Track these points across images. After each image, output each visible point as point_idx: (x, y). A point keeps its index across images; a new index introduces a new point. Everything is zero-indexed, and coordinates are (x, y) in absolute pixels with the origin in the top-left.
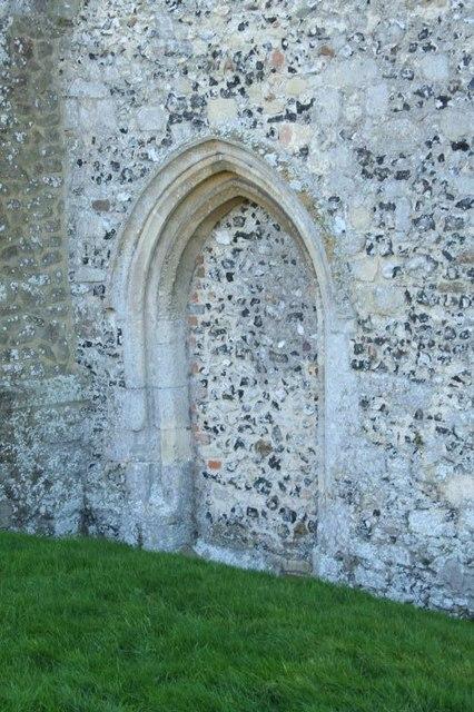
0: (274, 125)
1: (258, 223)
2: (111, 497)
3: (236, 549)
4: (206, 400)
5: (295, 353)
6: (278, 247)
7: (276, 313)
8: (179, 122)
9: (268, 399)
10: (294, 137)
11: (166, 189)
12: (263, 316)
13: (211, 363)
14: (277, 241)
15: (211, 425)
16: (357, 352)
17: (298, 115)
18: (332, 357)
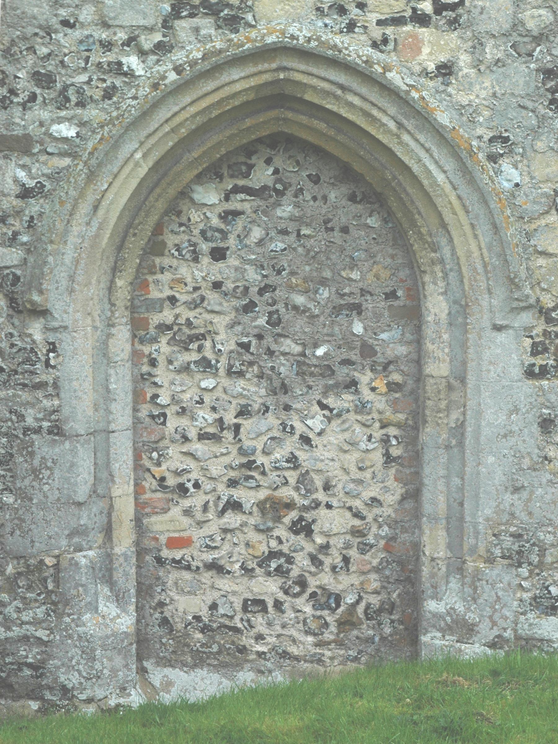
0: (389, 30)
1: (276, 171)
2: (26, 616)
3: (222, 667)
4: (161, 444)
5: (347, 362)
6: (314, 209)
7: (311, 305)
8: (192, 15)
9: (292, 433)
10: (426, 50)
11: (167, 121)
12: (283, 311)
13: (169, 385)
14: (315, 199)
15: (171, 481)
16: (534, 353)
17: (434, 17)
18: (491, 363)
